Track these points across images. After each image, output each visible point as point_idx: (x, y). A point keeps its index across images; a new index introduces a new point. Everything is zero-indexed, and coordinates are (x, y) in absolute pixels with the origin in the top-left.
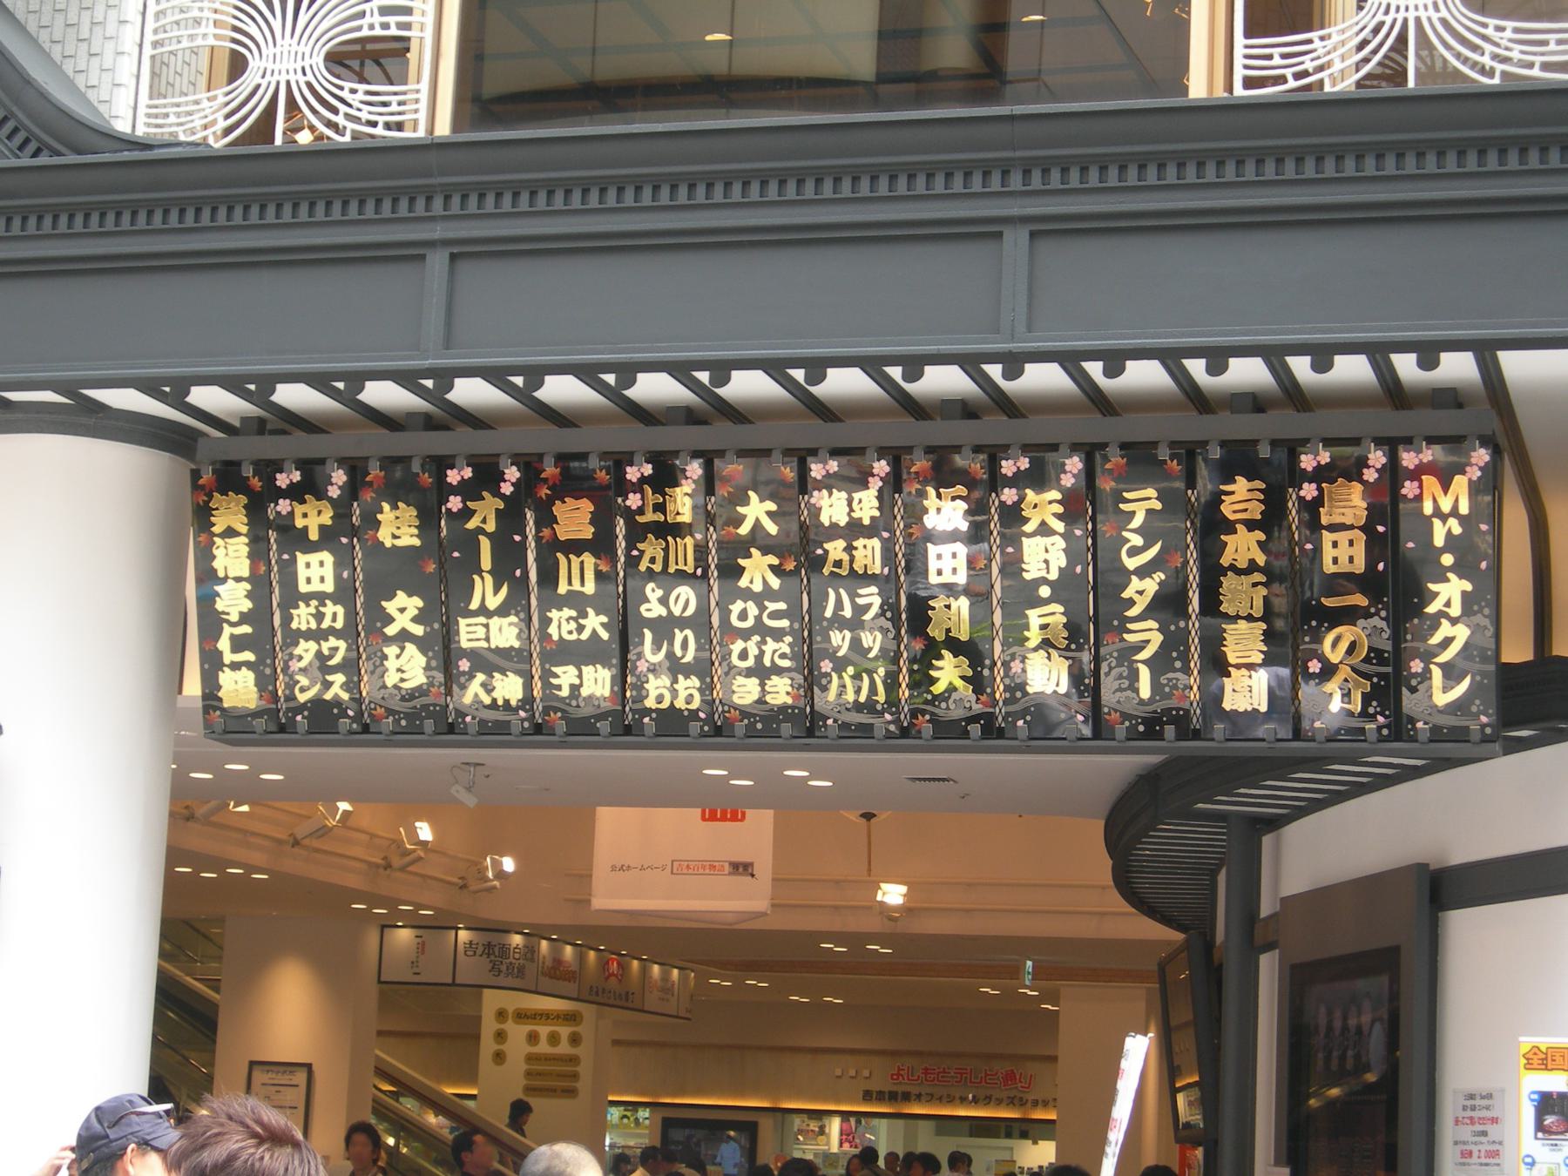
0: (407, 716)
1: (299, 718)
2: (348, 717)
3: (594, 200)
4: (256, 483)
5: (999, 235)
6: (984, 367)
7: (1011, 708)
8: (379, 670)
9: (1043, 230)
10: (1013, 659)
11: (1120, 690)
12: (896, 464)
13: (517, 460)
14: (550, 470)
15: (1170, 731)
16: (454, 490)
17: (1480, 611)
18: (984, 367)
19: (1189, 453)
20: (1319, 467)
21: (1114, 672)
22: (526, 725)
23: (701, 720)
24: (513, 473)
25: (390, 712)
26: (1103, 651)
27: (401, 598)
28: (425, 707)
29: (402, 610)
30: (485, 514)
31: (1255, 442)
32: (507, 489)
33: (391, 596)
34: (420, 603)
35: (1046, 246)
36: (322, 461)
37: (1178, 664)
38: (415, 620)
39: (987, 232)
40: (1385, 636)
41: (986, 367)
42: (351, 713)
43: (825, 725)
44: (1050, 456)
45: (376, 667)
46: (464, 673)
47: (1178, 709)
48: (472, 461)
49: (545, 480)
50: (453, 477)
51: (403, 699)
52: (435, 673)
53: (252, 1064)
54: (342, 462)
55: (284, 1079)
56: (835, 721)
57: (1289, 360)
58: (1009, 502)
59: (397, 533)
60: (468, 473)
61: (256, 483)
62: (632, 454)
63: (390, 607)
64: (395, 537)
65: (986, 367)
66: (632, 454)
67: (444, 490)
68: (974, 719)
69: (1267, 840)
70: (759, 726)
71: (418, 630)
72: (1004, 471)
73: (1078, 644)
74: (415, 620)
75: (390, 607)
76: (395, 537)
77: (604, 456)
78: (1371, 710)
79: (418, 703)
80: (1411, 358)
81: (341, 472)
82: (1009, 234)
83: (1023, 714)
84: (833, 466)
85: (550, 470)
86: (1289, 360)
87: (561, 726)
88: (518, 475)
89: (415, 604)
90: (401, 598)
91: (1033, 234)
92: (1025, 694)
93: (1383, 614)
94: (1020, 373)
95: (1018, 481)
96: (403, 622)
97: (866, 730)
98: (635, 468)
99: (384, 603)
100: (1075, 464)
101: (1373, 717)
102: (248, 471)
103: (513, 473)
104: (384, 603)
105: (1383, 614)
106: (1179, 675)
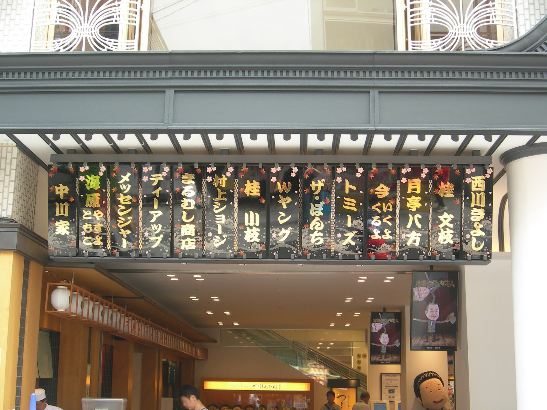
0: (316, 253)
1: (404, 254)
2: (294, 253)
3: (189, 75)
4: (199, 171)
5: (164, 92)
6: (47, 135)
7: (145, 247)
8: (436, 238)
9: (178, 90)
10: (145, 231)
11: (54, 240)
12: (236, 168)
13: (296, 165)
14: (439, 169)
15: (325, 256)
16: (274, 175)
17: (359, 219)
18: (47, 135)
19: (203, 166)
20: (342, 172)
21: (307, 237)
22: (232, 255)
23: (423, 254)
24: (295, 170)
25: (310, 251)
26: (175, 229)
27: (446, 215)
28: (323, 250)
29: (446, 219)
30: (93, 182)
31: (258, 164)
32: (423, 176)
33: (442, 214)
34: (452, 217)
35: (179, 95)
36: (98, 163)
37: (327, 235)
38: (450, 222)
39: (161, 90)
40: (362, 226)
41: (79, 135)
42: (295, 252)
43: (467, 256)
44: (175, 167)
45: (435, 237)
46: (210, 237)
47: (327, 249)
48: (216, 164)
49: (437, 173)
50: (404, 171)
51: (315, 247)
52: (457, 239)
53: (381, 374)
54: (232, 164)
55: (393, 378)
56: (341, 254)
57: (144, 135)
58: (209, 181)
59: (252, 191)
60: (409, 170)
61: (199, 171)
62: (339, 164)
63: (441, 218)
64: (445, 194)
65: (79, 135)
66: (339, 164)
67: (399, 176)
68: (389, 253)
69: (66, 288)
70: (315, 255)
71: (451, 226)
72: (467, 172)
73: (424, 229)
74: (450, 222)
75: (441, 218)
76: (251, 192)
77: (73, 163)
78: (485, 250)
79: (320, 248)
80: (282, 136)
81: (104, 167)
82: (372, 91)
83: (404, 252)
84: (474, 170)
85: (439, 169)
86: (144, 135)
87: (244, 256)
88: (105, 169)
89: (450, 217)
90: (446, 215)
91: (175, 91)
92: (406, 245)
93: (361, 219)
94: (189, 137)
95: (85, 173)
96: (445, 223)
97: (352, 257)
98: (340, 169)
99: (439, 217)
100: (167, 169)
101: (486, 252)
102: (196, 166)
103: (426, 171)
104: (439, 217)
105: (361, 219)
106: (327, 238)
